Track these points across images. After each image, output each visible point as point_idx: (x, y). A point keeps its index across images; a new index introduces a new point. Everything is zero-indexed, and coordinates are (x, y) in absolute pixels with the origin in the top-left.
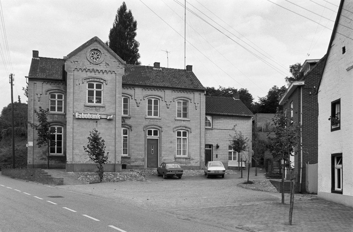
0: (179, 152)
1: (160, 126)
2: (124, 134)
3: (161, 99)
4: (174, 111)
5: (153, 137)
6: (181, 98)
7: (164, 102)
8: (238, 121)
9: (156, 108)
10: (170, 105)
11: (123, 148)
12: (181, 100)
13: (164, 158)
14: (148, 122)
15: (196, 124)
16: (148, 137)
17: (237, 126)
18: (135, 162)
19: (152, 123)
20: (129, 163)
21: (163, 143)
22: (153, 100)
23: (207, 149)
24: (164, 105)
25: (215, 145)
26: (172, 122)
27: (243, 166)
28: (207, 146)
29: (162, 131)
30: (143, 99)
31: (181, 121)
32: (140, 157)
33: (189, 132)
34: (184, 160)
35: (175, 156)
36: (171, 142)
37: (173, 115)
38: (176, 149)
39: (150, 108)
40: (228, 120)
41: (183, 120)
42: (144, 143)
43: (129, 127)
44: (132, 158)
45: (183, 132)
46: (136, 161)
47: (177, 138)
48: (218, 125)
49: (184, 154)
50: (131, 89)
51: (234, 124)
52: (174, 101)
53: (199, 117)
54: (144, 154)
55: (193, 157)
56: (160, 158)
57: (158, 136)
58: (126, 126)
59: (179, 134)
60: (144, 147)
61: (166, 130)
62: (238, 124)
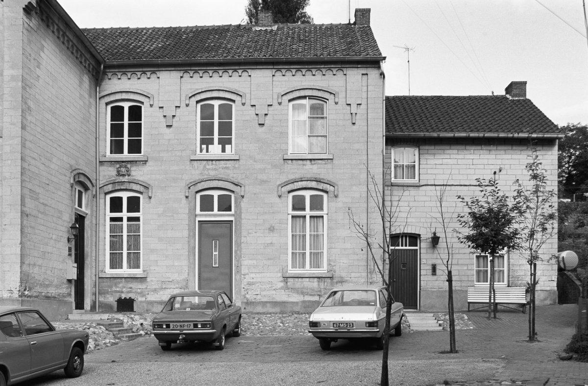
0: (298, 258)
1: (236, 181)
2: (294, 209)
3: (331, 97)
4: (281, 133)
5: (216, 215)
6: (302, 93)
7: (250, 108)
8: (509, 156)
9: (136, 130)
10: (174, 116)
11: (128, 250)
12: (304, 97)
13: (248, 279)
14: (198, 172)
15: (354, 171)
16: (200, 215)
17: (503, 172)
18: (161, 293)
19: (212, 173)
20: (142, 294)
21: (244, 233)
22: (216, 104)
23: (404, 248)
24: (248, 118)
25: (426, 234)
26: (275, 166)
27: (496, 301)
28: (395, 238)
29: (243, 197)
30: (275, 103)
31: (305, 162)
32: (175, 277)
33: (331, 195)
34: (315, 284)
35: (284, 270)
36: (272, 229)
37: (278, 145)
38: (290, 251)
39: (117, 130)
40: (471, 157)
41: (311, 160)
42: (186, 233)
43: (142, 189)
44: (152, 281)
45: (219, 196)
46: (162, 289)
47: (293, 217)
48: (435, 171)
49: (316, 263)
50: (314, 75)
51: (492, 167)
52: (280, 104)
53: (364, 147)
54: (186, 269)
55: (343, 275)
56: (238, 277)
57: (233, 212)
58: (135, 187)
59: (298, 204)
60: (186, 247)
61: (255, 194)
62: (507, 167)
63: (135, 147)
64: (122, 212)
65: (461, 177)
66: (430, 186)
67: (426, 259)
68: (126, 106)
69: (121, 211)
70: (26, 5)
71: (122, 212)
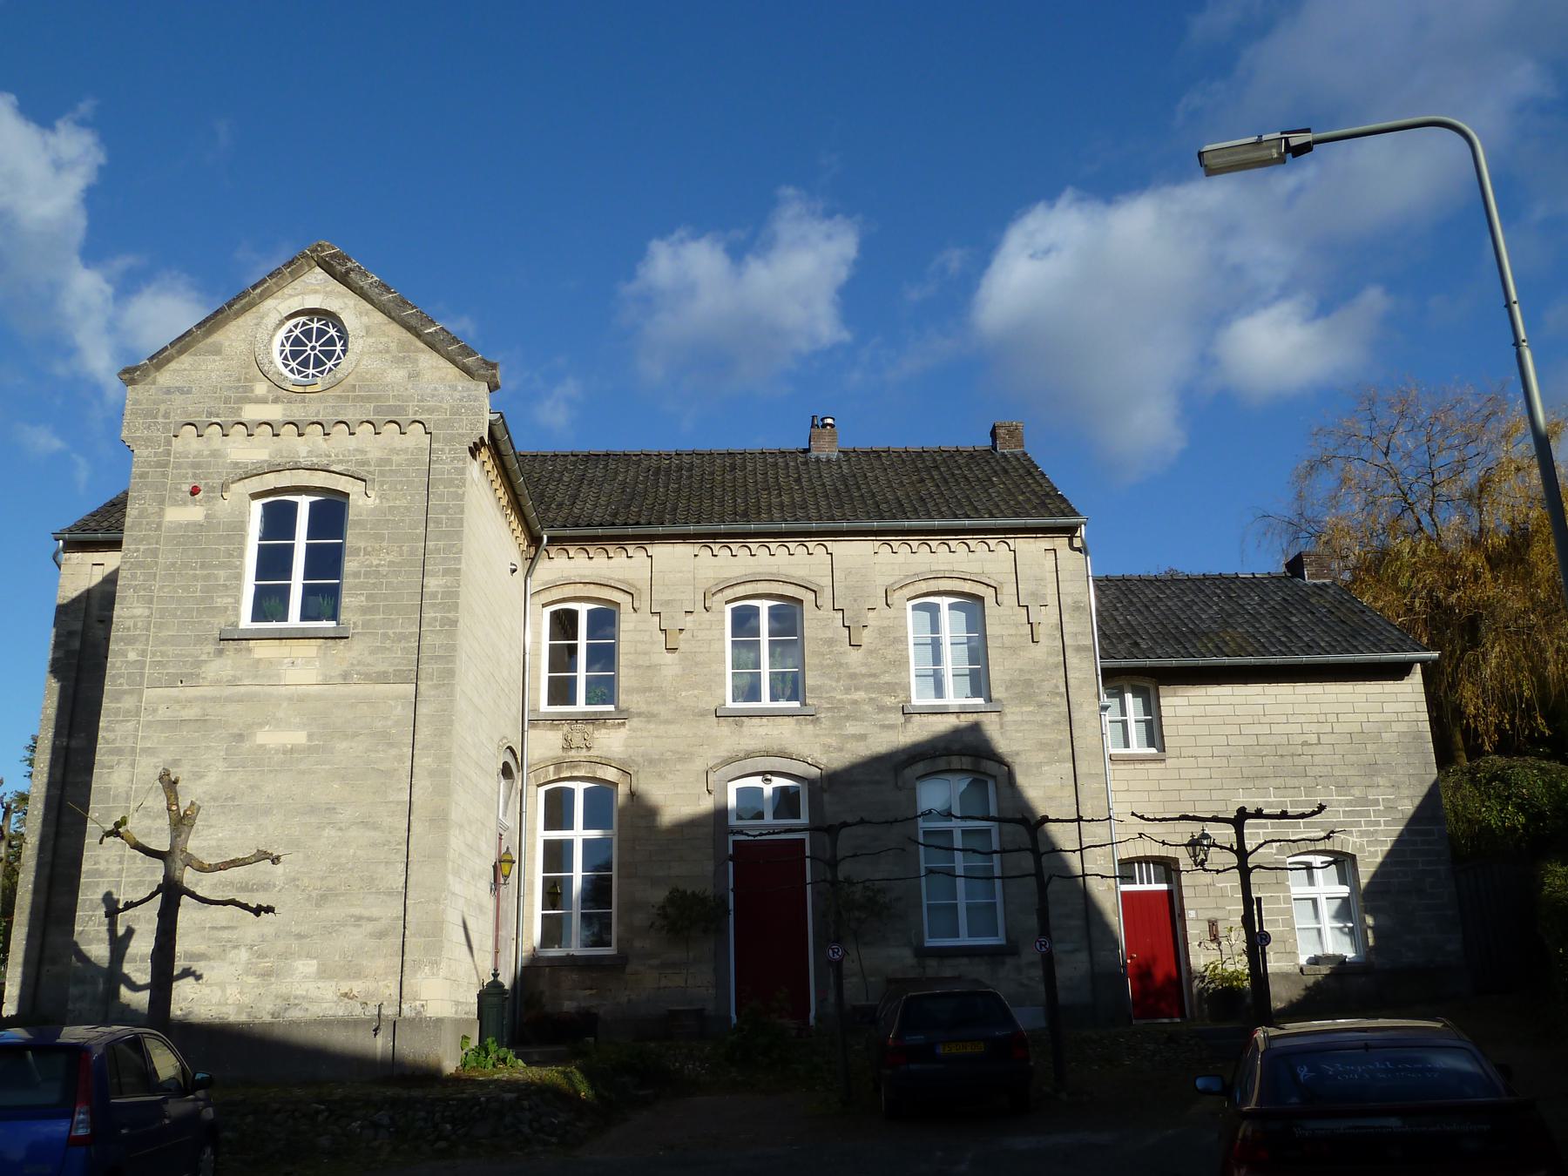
9: (603, 656)
63: (603, 690)
64: (573, 829)
65: (1261, 700)
66: (1079, 799)
67: (1196, 910)
68: (583, 609)
69: (585, 828)
70: (474, 443)
71: (573, 829)
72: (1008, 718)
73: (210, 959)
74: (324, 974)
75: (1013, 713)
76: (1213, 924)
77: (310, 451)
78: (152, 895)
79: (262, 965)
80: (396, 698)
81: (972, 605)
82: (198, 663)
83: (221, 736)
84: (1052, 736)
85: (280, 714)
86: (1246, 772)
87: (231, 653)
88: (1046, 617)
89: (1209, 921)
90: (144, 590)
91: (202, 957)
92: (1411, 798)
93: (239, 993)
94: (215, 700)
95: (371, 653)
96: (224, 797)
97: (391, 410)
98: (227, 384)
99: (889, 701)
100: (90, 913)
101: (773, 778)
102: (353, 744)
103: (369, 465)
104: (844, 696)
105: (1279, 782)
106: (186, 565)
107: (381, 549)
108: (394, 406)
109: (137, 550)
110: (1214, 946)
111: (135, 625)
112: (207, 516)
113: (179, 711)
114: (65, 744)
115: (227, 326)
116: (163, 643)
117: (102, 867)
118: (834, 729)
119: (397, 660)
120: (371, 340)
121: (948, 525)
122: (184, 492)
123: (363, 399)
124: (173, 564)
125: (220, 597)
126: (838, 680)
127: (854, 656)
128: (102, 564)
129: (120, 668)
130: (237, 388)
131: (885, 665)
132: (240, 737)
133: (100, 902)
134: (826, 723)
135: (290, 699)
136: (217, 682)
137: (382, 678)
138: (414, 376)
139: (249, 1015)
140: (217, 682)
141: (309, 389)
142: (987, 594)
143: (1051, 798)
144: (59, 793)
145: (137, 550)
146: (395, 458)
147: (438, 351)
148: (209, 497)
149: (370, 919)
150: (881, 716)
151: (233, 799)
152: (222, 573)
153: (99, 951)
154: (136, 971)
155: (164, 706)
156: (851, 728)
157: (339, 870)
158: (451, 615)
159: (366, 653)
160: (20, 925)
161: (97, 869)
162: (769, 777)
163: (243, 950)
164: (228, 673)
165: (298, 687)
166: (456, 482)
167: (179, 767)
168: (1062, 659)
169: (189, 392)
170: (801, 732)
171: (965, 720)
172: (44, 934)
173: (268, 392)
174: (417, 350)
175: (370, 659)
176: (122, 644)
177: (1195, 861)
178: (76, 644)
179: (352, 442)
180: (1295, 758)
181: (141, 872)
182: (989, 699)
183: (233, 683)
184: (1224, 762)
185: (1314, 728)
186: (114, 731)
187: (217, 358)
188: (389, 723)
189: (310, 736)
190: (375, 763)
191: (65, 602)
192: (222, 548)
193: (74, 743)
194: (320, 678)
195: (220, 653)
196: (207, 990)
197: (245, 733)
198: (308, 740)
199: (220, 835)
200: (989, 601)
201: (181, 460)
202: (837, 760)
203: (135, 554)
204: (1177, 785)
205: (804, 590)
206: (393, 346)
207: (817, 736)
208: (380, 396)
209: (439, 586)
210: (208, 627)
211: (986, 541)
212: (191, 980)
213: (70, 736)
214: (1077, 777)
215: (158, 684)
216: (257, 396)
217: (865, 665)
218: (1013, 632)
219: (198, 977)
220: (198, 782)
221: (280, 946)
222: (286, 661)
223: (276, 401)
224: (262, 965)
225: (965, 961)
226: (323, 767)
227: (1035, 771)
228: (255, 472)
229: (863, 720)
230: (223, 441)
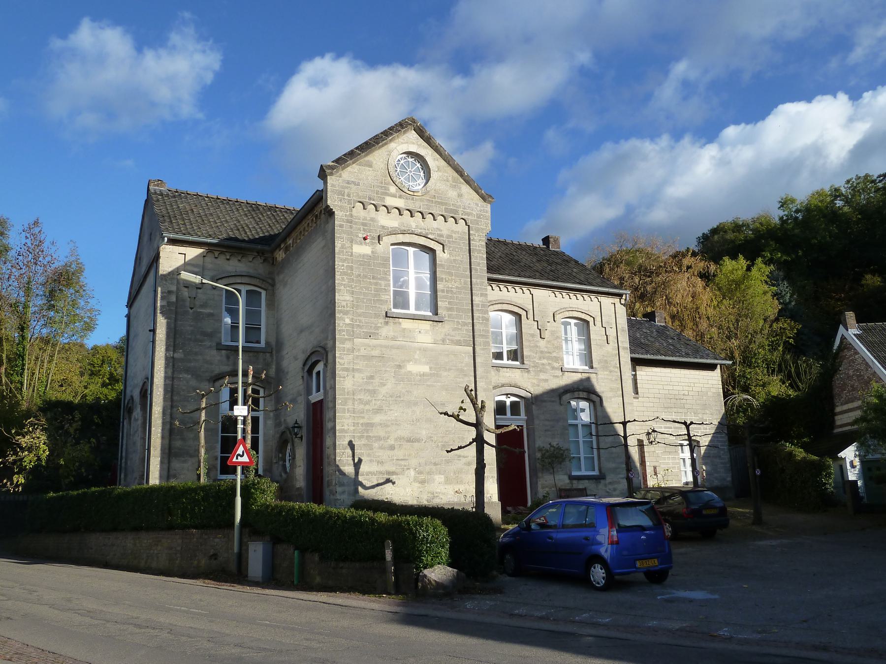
65: (670, 375)
72: (599, 376)
73: (397, 475)
74: (448, 481)
75: (602, 374)
76: (655, 468)
77: (416, 226)
78: (471, 443)
79: (420, 478)
80: (465, 353)
81: (584, 325)
82: (377, 328)
83: (391, 365)
84: (615, 386)
85: (416, 357)
86: (666, 405)
87: (392, 324)
88: (612, 333)
89: (654, 467)
90: (349, 287)
91: (393, 473)
92: (717, 419)
93: (412, 491)
94: (386, 347)
95: (453, 330)
96: (396, 396)
97: (452, 211)
98: (376, 184)
99: (556, 365)
100: (343, 451)
101: (511, 397)
102: (450, 374)
103: (443, 237)
104: (539, 361)
105: (675, 410)
106: (366, 277)
107: (452, 280)
108: (453, 209)
109: (343, 266)
110: (655, 477)
111: (347, 304)
112: (372, 252)
113: (370, 351)
114: (172, 355)
115: (374, 153)
116: (360, 316)
117: (346, 427)
118: (535, 376)
119: (464, 335)
120: (440, 174)
121: (546, 283)
122: (360, 238)
123: (439, 203)
124: (360, 275)
125: (384, 295)
126: (536, 353)
127: (542, 343)
128: (179, 253)
129: (342, 327)
130: (382, 187)
131: (554, 348)
132: (399, 367)
133: (347, 445)
134: (532, 373)
135: (420, 349)
136: (387, 338)
137: (458, 343)
138: (460, 196)
139: (417, 501)
140: (387, 338)
141: (415, 194)
142: (523, 313)
143: (615, 412)
144: (171, 383)
145: (343, 266)
146: (454, 235)
147: (470, 185)
148: (372, 242)
149: (464, 457)
150: (553, 371)
151: (400, 397)
152: (383, 283)
153: (349, 469)
154: (364, 480)
155: (363, 348)
156: (543, 376)
157: (449, 434)
158: (486, 316)
159: (451, 330)
160: (155, 457)
161: (344, 429)
162: (509, 396)
163: (412, 470)
164: (391, 334)
165: (423, 344)
166: (482, 252)
167: (373, 379)
168: (617, 352)
169: (358, 185)
170: (523, 376)
171: (585, 376)
172: (169, 462)
173: (396, 192)
174: (461, 183)
175: (453, 333)
176: (342, 314)
177: (649, 441)
178: (173, 298)
179: (435, 224)
180: (681, 400)
181: (362, 431)
182: (592, 367)
183: (394, 339)
184: (657, 400)
185: (687, 388)
186: (343, 359)
187: (370, 169)
188: (463, 365)
189: (430, 368)
190: (459, 383)
191: (164, 273)
192: (382, 269)
193: (176, 355)
194: (432, 340)
195: (387, 323)
196: (397, 489)
197: (402, 365)
198: (430, 370)
199: (396, 414)
200: (591, 324)
201: (356, 220)
202: (537, 390)
203: (342, 268)
204: (642, 409)
205: (522, 310)
206: (450, 178)
207: (529, 379)
208: (447, 203)
209: (480, 301)
210: (379, 309)
211: (569, 294)
212: (390, 484)
213: (174, 351)
214: (625, 404)
215: (359, 337)
216: (391, 193)
217: (546, 347)
218: (600, 338)
219: (394, 483)
220: (383, 387)
221: (427, 468)
222: (417, 330)
223: (400, 197)
224: (420, 478)
225: (587, 481)
226: (438, 384)
227: (609, 401)
228: (394, 233)
229: (546, 373)
230: (376, 214)
